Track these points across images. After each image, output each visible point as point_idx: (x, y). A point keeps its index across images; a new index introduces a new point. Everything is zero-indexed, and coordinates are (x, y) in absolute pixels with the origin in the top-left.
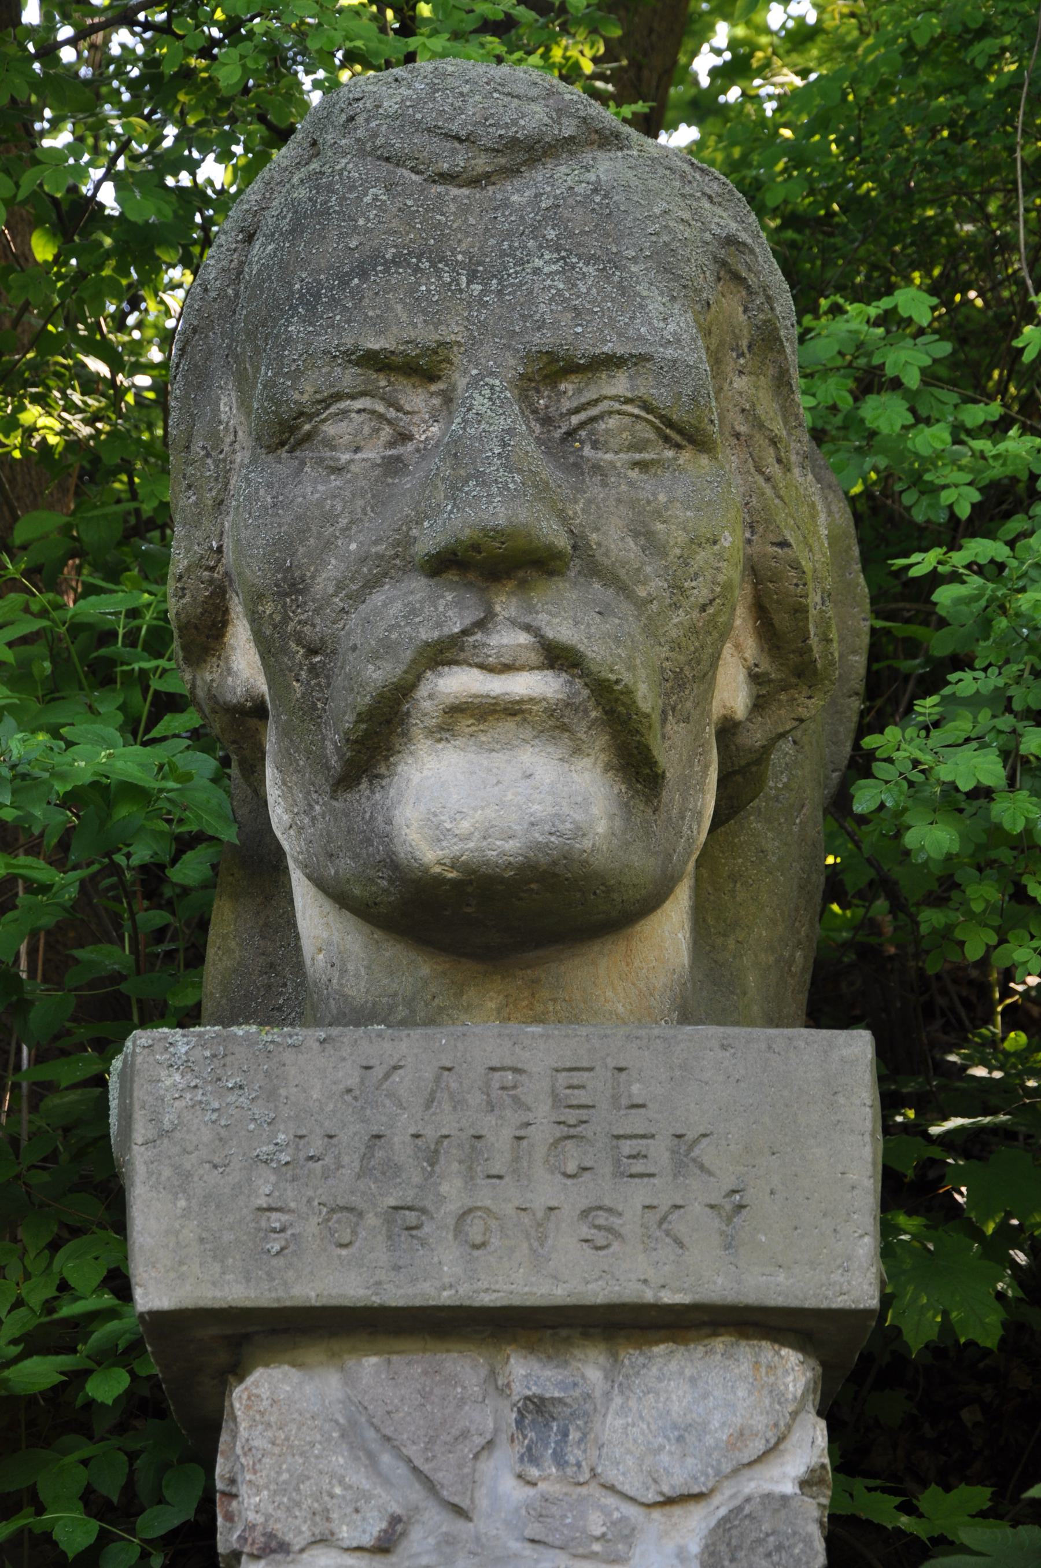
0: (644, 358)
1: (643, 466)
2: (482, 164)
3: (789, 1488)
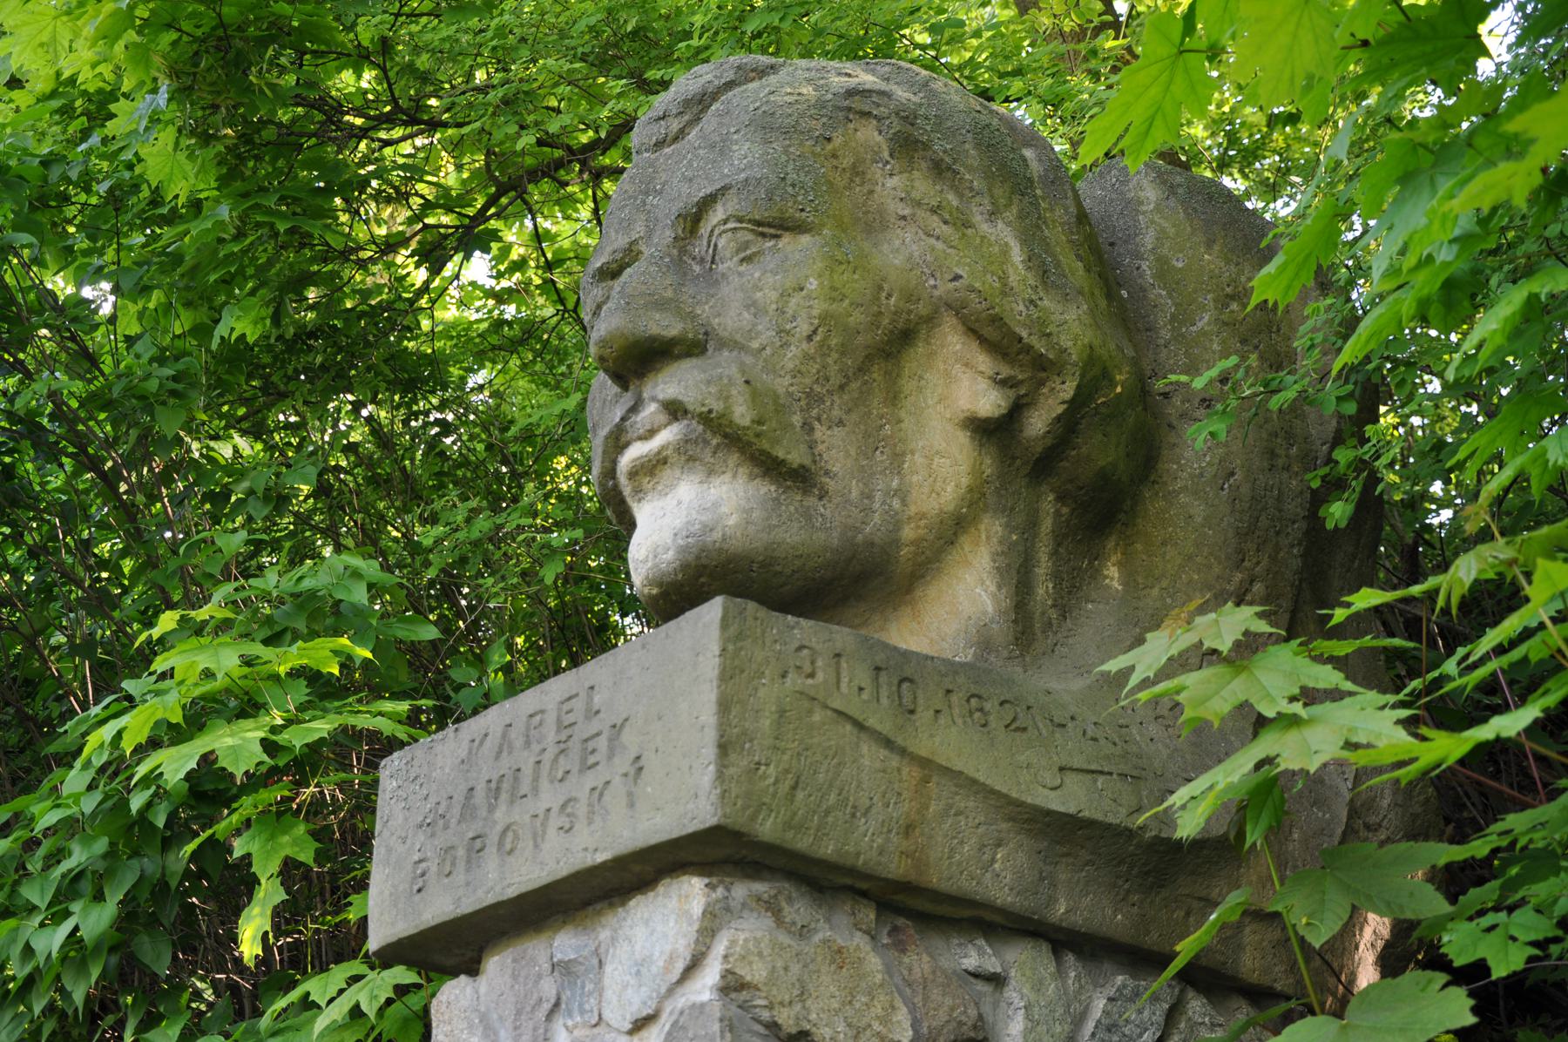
0: (725, 189)
2: (675, 125)
3: (706, 996)
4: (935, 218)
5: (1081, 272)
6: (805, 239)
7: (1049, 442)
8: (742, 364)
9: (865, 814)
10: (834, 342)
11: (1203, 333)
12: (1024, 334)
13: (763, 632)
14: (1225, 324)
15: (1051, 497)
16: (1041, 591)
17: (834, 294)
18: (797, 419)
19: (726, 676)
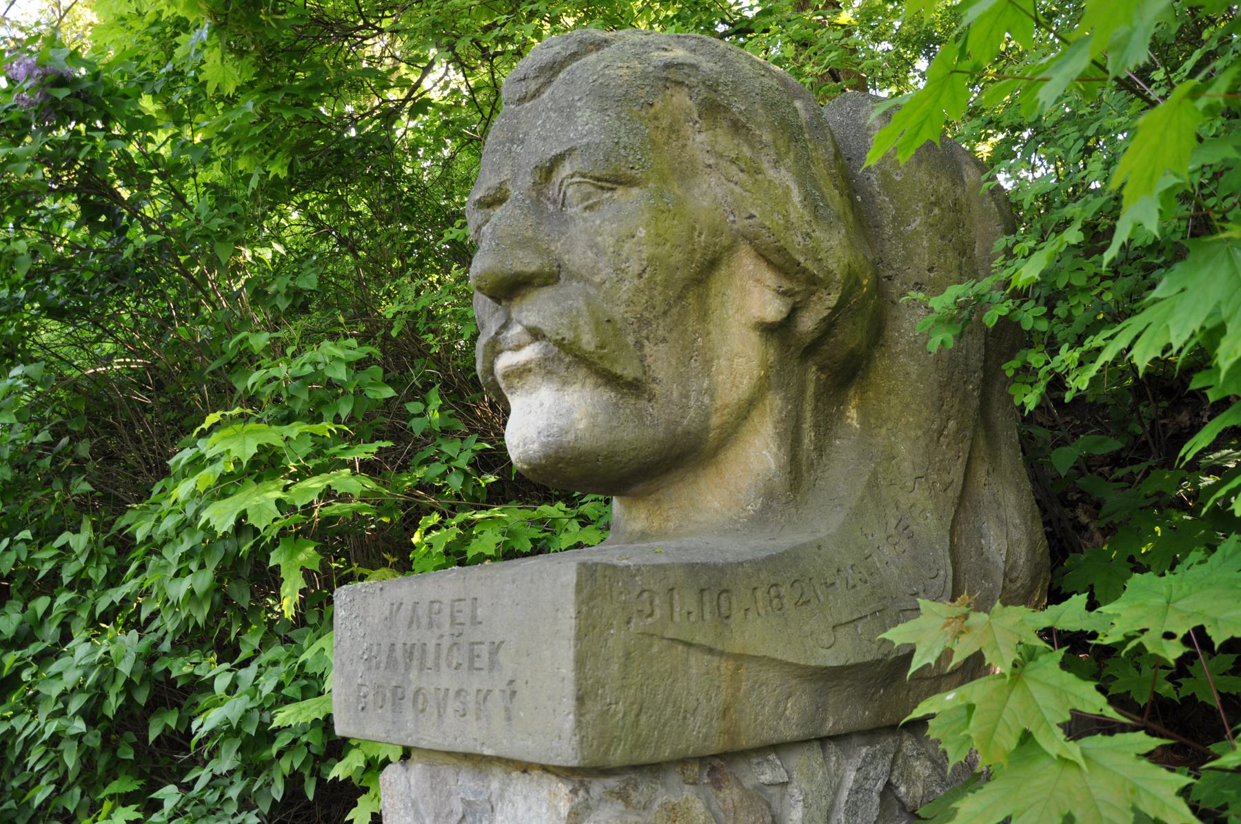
0: (571, 151)
1: (590, 208)
2: (533, 86)
4: (734, 167)
5: (838, 198)
6: (635, 191)
7: (816, 335)
8: (587, 295)
9: (693, 714)
10: (659, 278)
11: (916, 232)
12: (802, 260)
13: (611, 586)
14: (932, 226)
15: (814, 369)
16: (806, 441)
17: (659, 240)
18: (630, 340)
19: (580, 636)
